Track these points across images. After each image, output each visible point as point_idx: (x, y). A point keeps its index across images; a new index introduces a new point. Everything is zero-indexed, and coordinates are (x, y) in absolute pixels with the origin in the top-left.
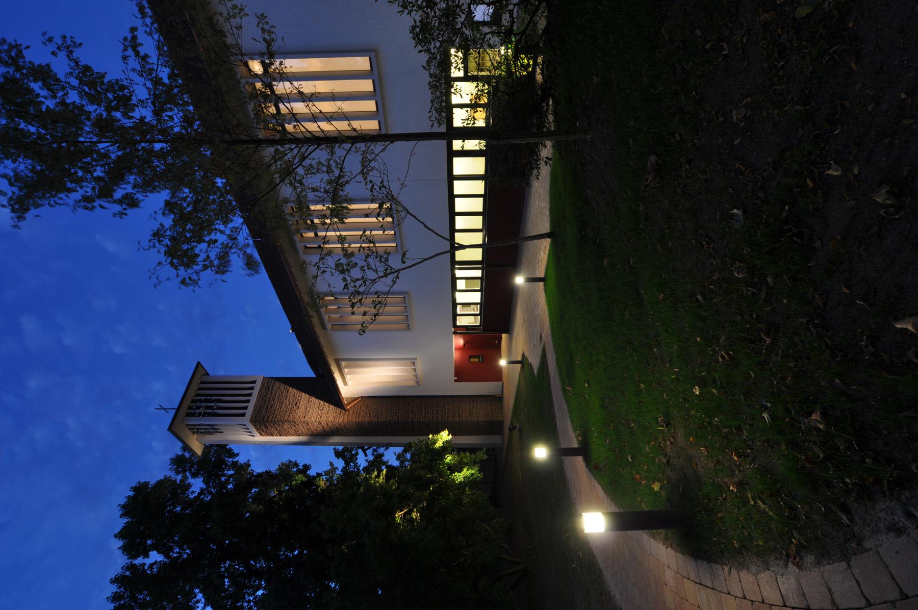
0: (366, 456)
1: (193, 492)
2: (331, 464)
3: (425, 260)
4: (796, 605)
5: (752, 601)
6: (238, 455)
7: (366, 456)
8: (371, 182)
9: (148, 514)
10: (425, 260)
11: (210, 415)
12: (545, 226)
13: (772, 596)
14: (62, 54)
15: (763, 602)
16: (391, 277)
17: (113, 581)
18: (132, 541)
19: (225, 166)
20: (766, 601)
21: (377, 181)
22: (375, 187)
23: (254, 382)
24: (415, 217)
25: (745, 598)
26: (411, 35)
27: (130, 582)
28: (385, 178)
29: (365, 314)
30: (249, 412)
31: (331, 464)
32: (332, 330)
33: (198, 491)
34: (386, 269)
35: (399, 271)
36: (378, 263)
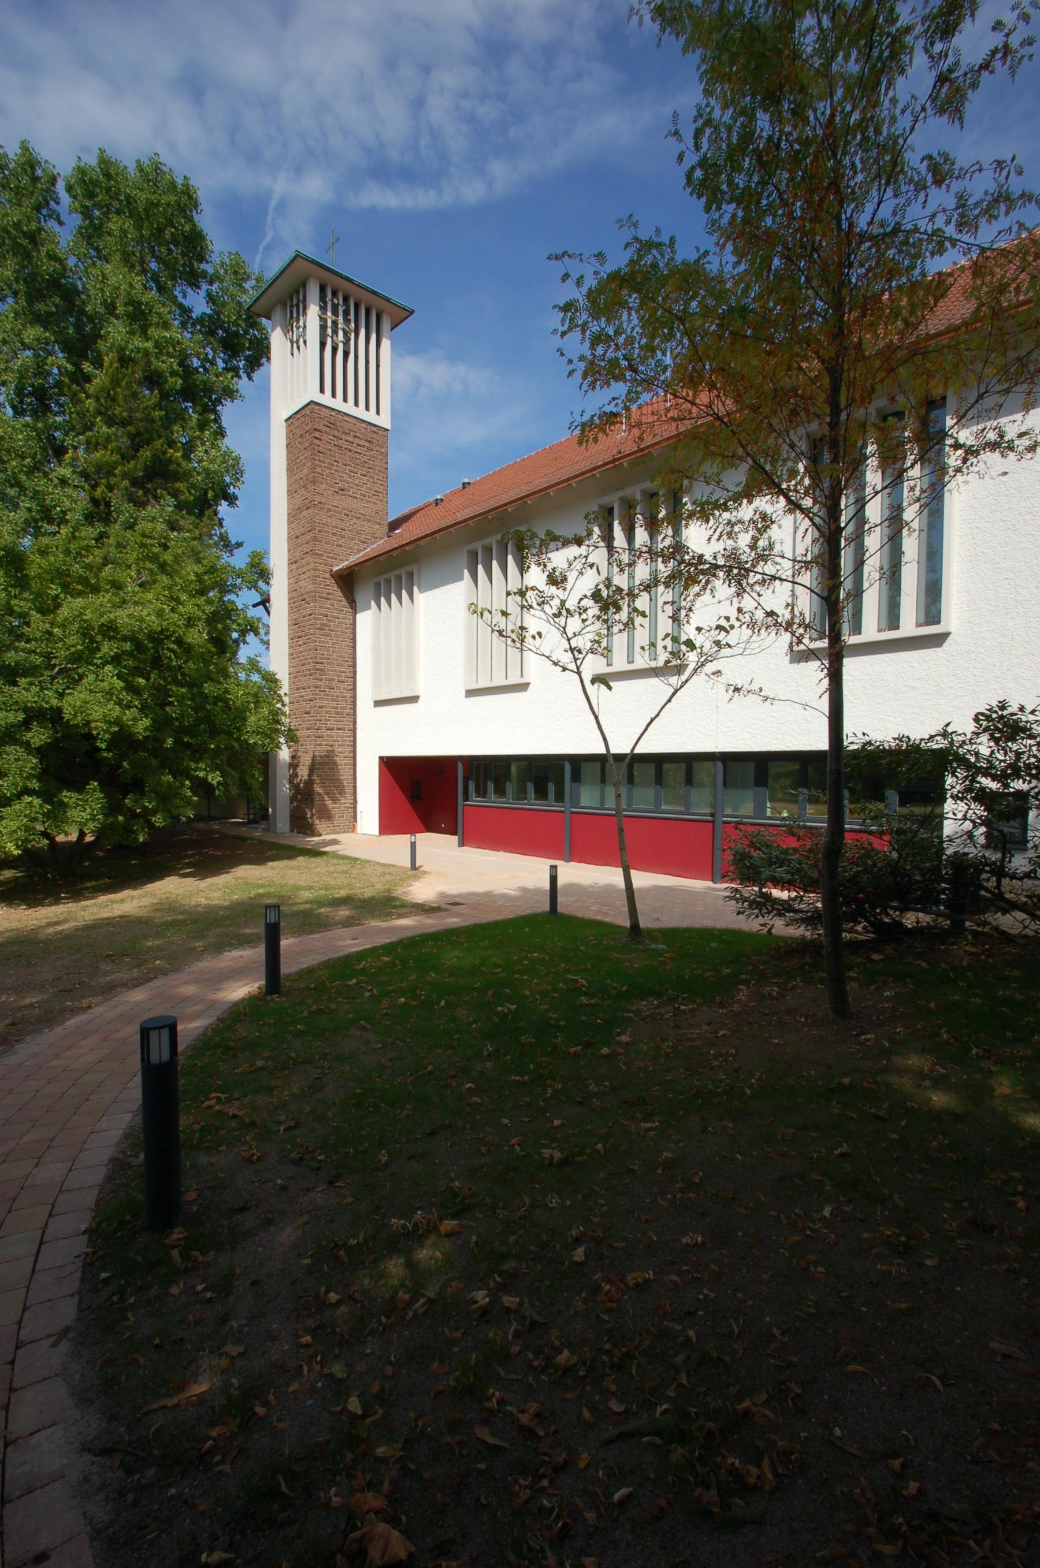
0: (254, 606)
1: (185, 297)
2: (239, 545)
3: (596, 718)
4: (9, 1470)
5: (13, 1362)
6: (250, 378)
7: (254, 606)
8: (732, 627)
9: (152, 219)
10: (596, 718)
11: (323, 328)
12: (612, 876)
13: (26, 1412)
14: (997, 40)
15: (12, 1390)
16: (566, 658)
17: (25, 147)
18: (101, 187)
19: (791, 361)
20: (14, 1396)
21: (732, 638)
22: (723, 634)
23: (378, 413)
24: (669, 701)
25: (17, 1348)
26: (994, 703)
27: (26, 179)
28: (737, 650)
29: (505, 614)
30: (326, 399)
31: (239, 545)
32: (470, 552)
33: (186, 303)
34: (580, 651)
35: (579, 673)
36: (591, 636)
